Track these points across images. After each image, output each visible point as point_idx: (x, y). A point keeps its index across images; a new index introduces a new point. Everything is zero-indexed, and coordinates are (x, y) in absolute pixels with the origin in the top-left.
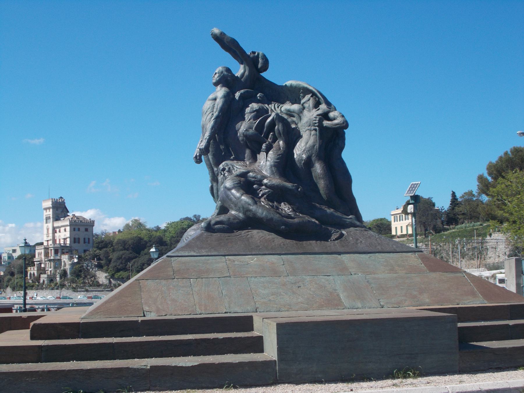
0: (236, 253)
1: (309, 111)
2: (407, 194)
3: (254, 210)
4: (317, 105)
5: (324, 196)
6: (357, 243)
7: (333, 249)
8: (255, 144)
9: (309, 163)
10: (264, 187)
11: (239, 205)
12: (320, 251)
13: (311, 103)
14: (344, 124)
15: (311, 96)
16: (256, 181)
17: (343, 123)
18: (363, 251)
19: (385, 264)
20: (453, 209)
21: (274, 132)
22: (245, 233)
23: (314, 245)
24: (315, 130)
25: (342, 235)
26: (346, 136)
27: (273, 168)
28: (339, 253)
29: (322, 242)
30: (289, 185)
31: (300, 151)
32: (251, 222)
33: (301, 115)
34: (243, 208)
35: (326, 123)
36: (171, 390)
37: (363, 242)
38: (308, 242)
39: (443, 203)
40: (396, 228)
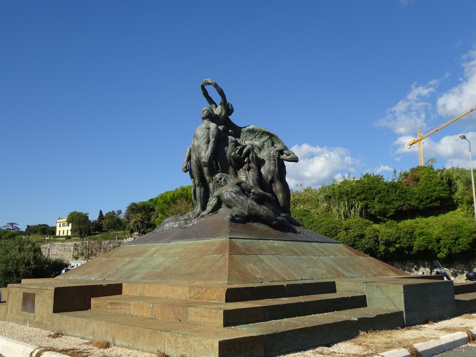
5: (282, 204)
8: (238, 164)
15: (269, 138)
20: (100, 221)
36: (285, 354)
39: (93, 217)
40: (60, 231)
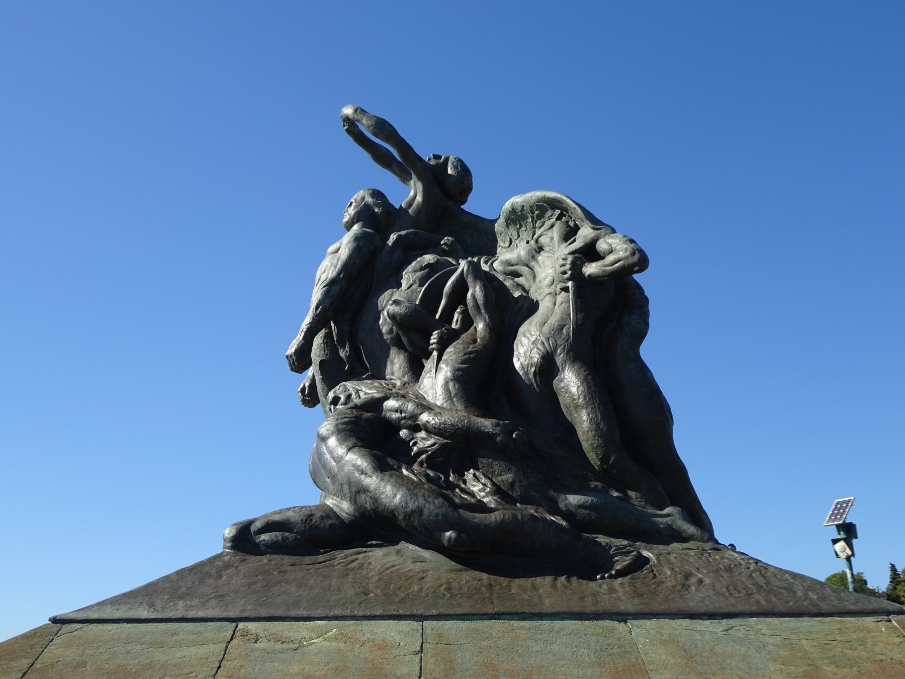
0: (279, 613)
1: (552, 251)
2: (828, 521)
3: (372, 487)
4: (570, 234)
5: (593, 458)
6: (686, 587)
7: (605, 603)
8: (417, 337)
9: (547, 368)
10: (422, 434)
11: (341, 477)
12: (557, 609)
13: (556, 233)
14: (637, 256)
16: (404, 418)
17: (633, 254)
18: (703, 609)
19: (784, 653)
20: (895, 589)
21: (466, 305)
22: (346, 557)
23: (545, 589)
24: (566, 289)
25: (641, 562)
26: (651, 307)
27: (451, 384)
28: (623, 617)
29: (574, 579)
30: (487, 424)
31: (526, 351)
32: (371, 526)
33: (533, 264)
34: (349, 484)
35: (591, 269)
37: (707, 581)
38: (528, 582)
